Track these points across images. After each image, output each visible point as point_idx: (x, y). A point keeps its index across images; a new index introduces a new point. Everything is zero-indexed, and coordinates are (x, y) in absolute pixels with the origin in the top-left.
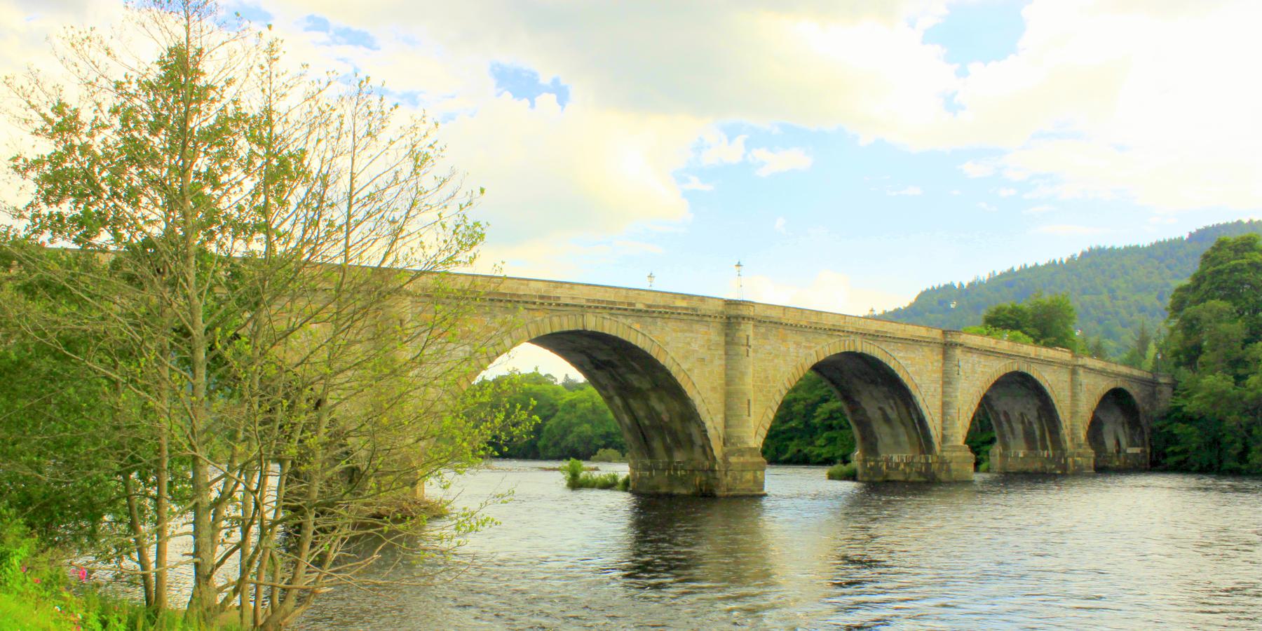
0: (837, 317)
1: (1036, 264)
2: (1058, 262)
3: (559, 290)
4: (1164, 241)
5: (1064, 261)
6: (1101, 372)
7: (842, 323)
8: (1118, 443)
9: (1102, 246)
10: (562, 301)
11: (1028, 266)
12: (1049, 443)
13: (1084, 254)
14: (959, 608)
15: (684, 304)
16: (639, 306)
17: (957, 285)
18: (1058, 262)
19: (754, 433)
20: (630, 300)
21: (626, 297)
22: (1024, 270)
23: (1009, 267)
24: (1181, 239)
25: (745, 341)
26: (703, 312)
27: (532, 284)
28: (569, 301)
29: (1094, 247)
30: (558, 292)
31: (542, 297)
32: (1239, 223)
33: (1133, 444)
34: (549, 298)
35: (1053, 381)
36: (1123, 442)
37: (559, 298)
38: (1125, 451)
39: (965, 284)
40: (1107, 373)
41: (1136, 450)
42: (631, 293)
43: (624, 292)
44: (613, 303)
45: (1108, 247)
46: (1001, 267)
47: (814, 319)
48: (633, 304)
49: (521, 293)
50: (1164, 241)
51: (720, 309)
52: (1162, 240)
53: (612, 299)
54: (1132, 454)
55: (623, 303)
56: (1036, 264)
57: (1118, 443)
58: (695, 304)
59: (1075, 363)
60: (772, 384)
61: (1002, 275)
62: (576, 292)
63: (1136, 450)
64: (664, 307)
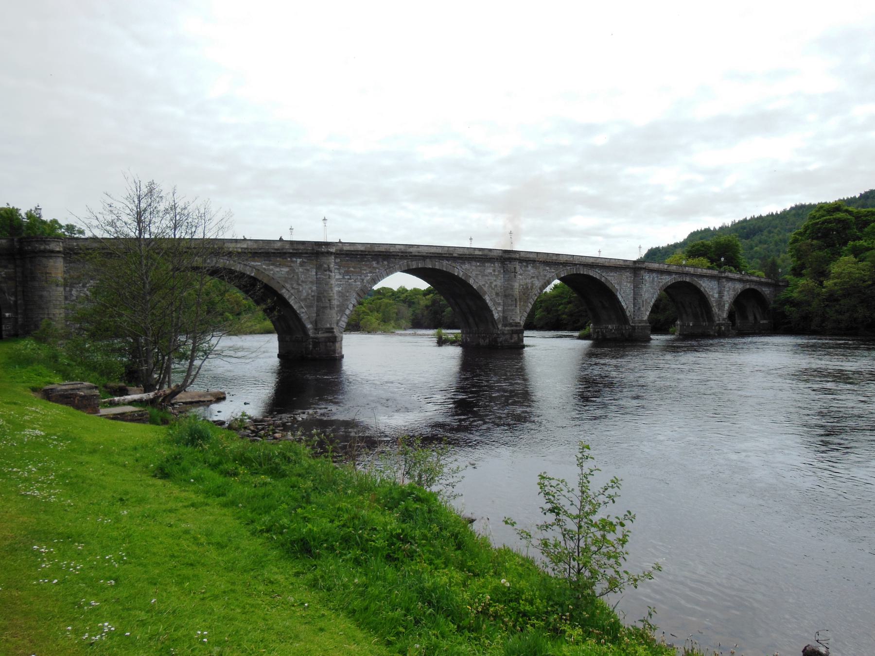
0: (569, 256)
1: (861, 194)
2: (774, 214)
3: (411, 249)
4: (698, 230)
5: (779, 213)
6: (740, 280)
7: (571, 259)
8: (755, 318)
9: (803, 203)
10: (413, 254)
11: (756, 217)
12: (706, 318)
13: (792, 208)
14: (738, 424)
15: (480, 253)
16: (455, 255)
17: (712, 229)
18: (774, 214)
19: (646, 315)
20: (450, 252)
21: (447, 251)
22: (753, 219)
23: (744, 218)
24: (855, 197)
25: (514, 270)
26: (490, 257)
27: (397, 246)
28: (417, 254)
29: (798, 204)
30: (411, 250)
31: (402, 252)
32: (745, 220)
33: (765, 319)
34: (406, 252)
35: (709, 288)
36: (758, 317)
37: (411, 252)
38: (759, 323)
39: (717, 228)
40: (743, 280)
41: (765, 322)
42: (450, 249)
43: (447, 248)
44: (442, 254)
45: (807, 203)
46: (738, 218)
47: (554, 258)
48: (452, 254)
49: (391, 251)
50: (698, 230)
51: (501, 254)
52: (696, 230)
53: (440, 252)
54: (763, 324)
55: (446, 254)
56: (861, 194)
57: (755, 318)
58: (486, 252)
59: (721, 275)
60: (530, 291)
61: (740, 222)
62: (420, 249)
63: (765, 322)
64: (469, 255)
